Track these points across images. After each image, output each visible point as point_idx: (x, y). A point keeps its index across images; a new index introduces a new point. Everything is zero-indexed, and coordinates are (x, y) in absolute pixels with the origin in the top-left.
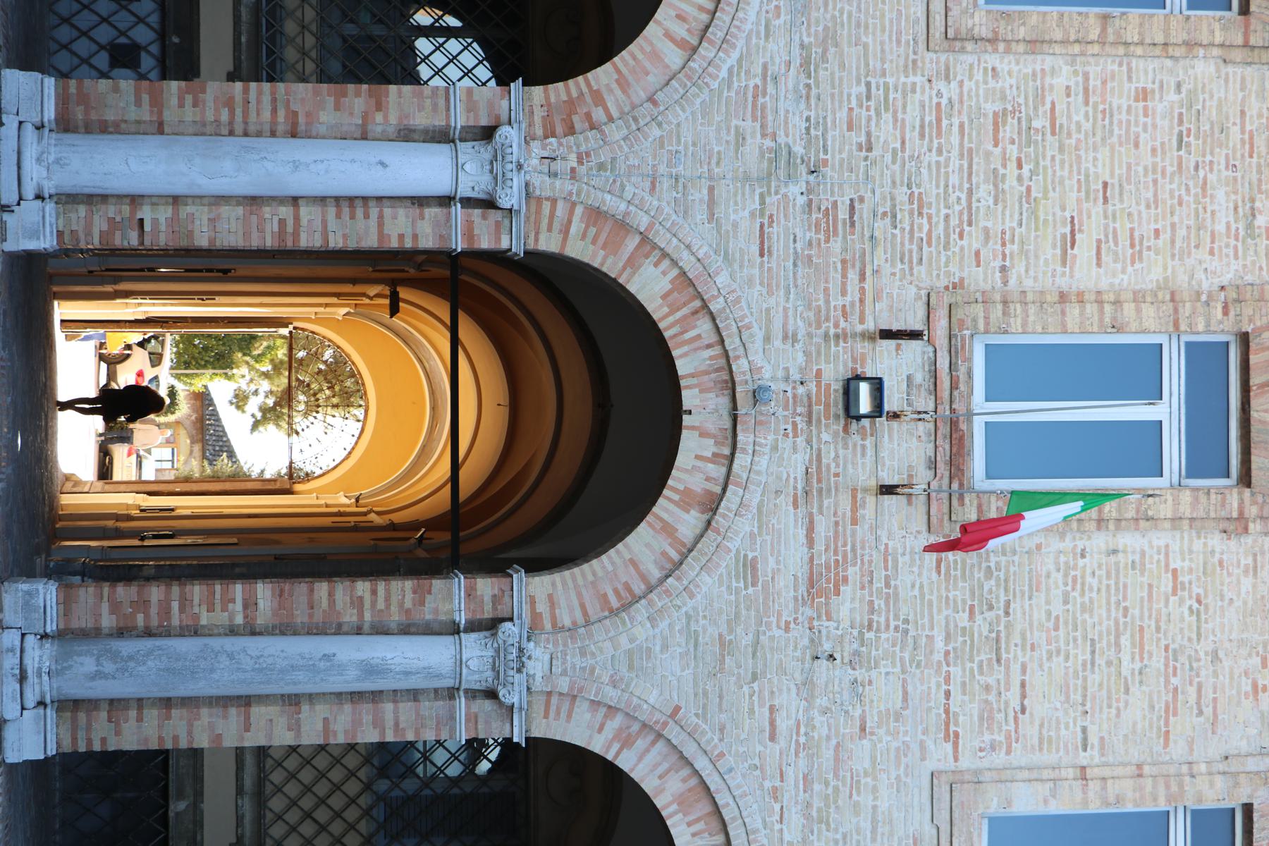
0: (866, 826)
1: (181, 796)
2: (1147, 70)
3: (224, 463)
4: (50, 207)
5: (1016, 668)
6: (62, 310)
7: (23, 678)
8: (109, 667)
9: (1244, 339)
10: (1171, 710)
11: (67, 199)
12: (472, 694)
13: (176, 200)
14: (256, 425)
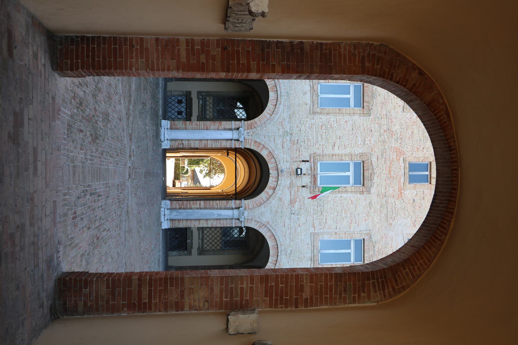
0: (300, 241)
1: (189, 239)
2: (347, 118)
3: (198, 185)
4: (169, 141)
5: (325, 216)
6: (168, 155)
7: (165, 215)
8: (178, 214)
9: (363, 162)
10: (351, 223)
11: (172, 140)
12: (235, 219)
13: (188, 140)
14: (204, 177)
